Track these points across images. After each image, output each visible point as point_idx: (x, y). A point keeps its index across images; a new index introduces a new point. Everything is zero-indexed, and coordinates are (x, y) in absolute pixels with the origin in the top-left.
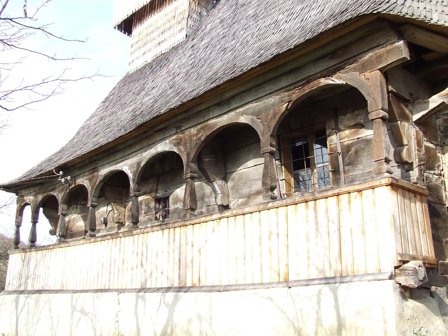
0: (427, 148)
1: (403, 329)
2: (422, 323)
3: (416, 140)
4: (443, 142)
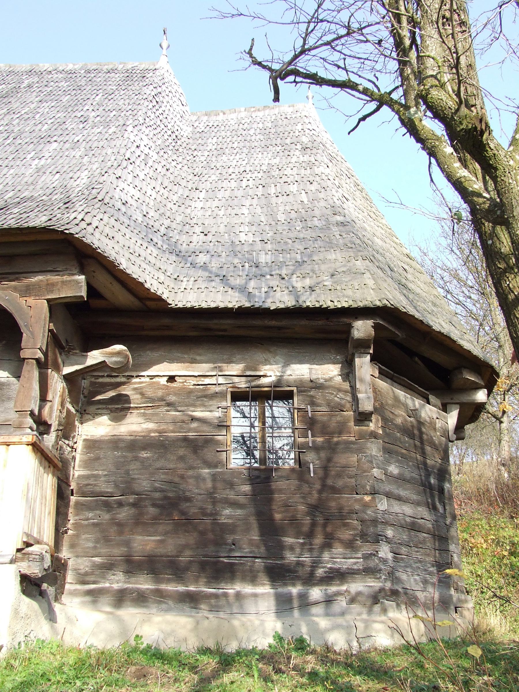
0: (68, 411)
1: (15, 629)
2: (33, 625)
3: (61, 398)
4: (84, 409)
